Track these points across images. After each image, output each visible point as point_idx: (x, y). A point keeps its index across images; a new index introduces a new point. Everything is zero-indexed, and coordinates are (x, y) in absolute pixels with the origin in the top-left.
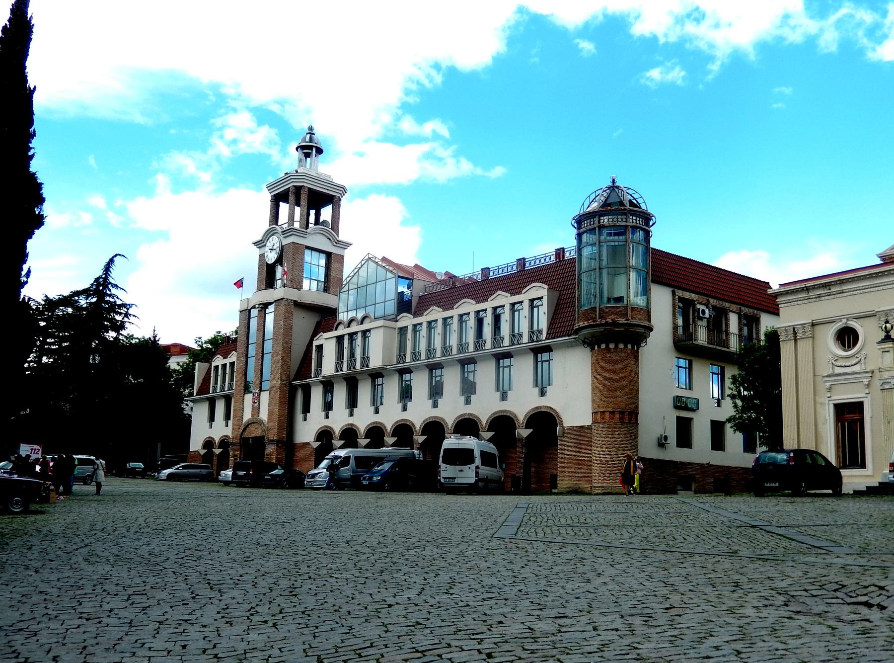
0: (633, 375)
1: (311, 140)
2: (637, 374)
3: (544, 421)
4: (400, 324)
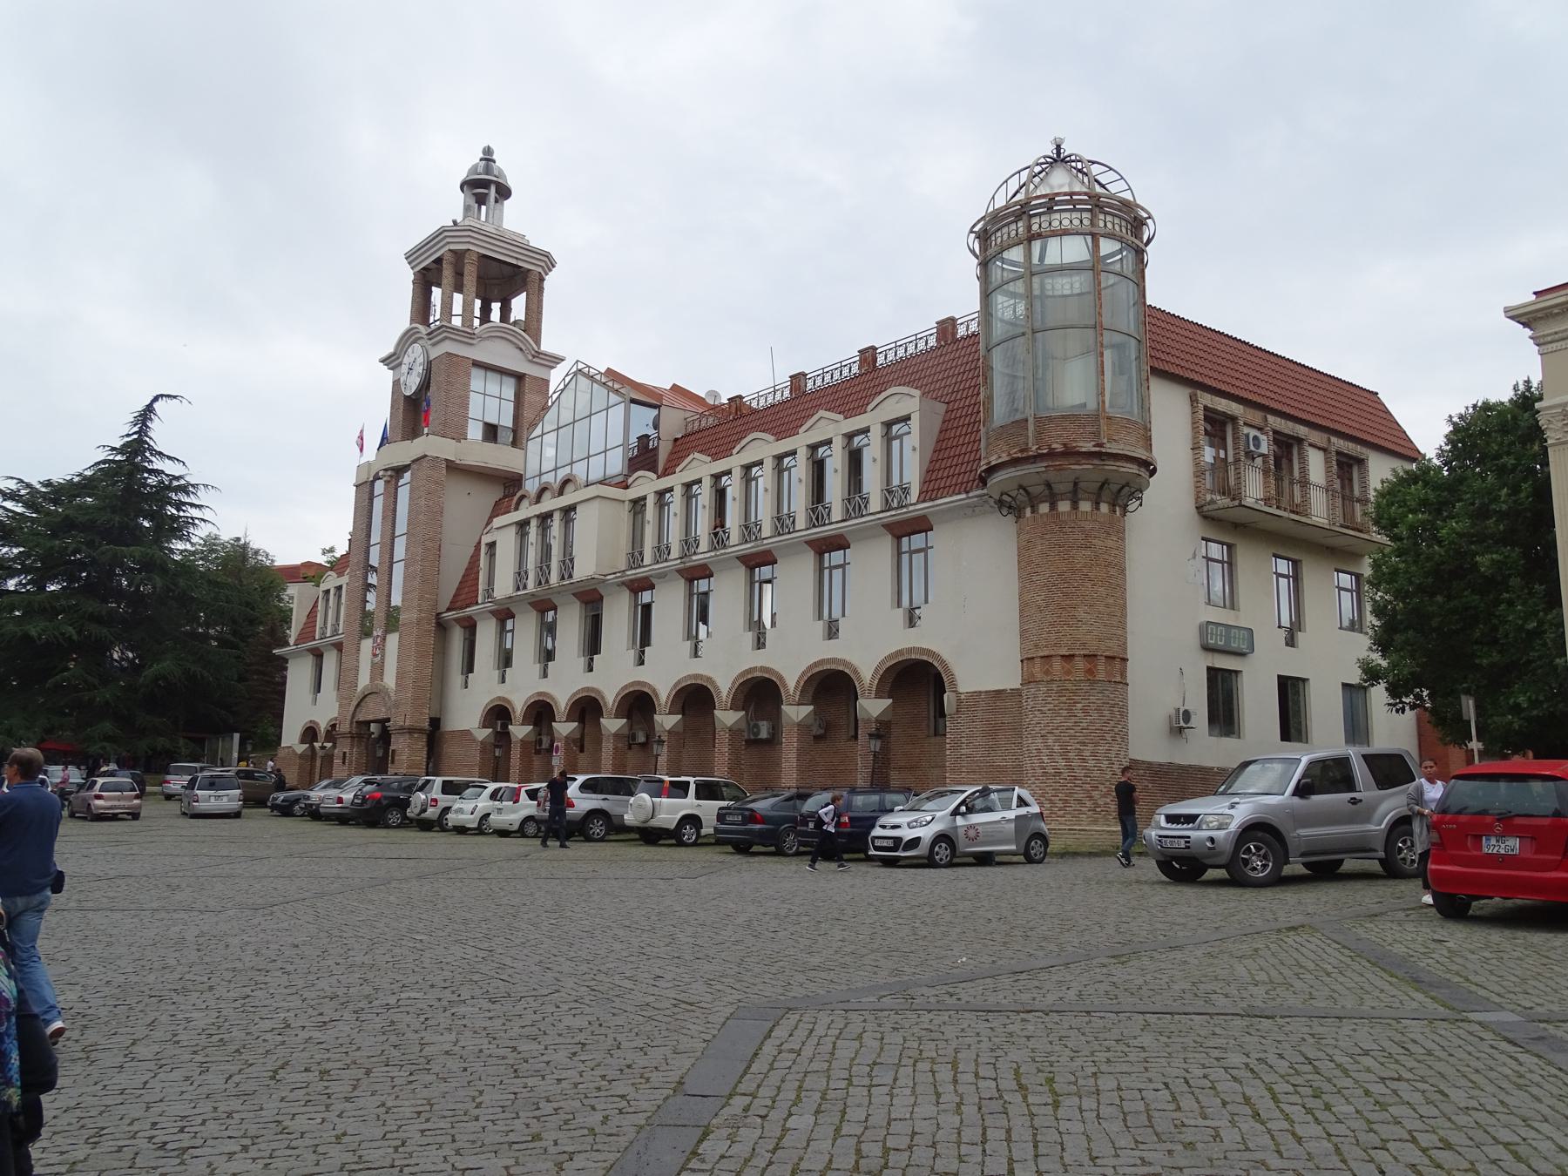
0: (1112, 571)
1: (488, 170)
2: (1122, 571)
3: (916, 679)
4: (633, 493)
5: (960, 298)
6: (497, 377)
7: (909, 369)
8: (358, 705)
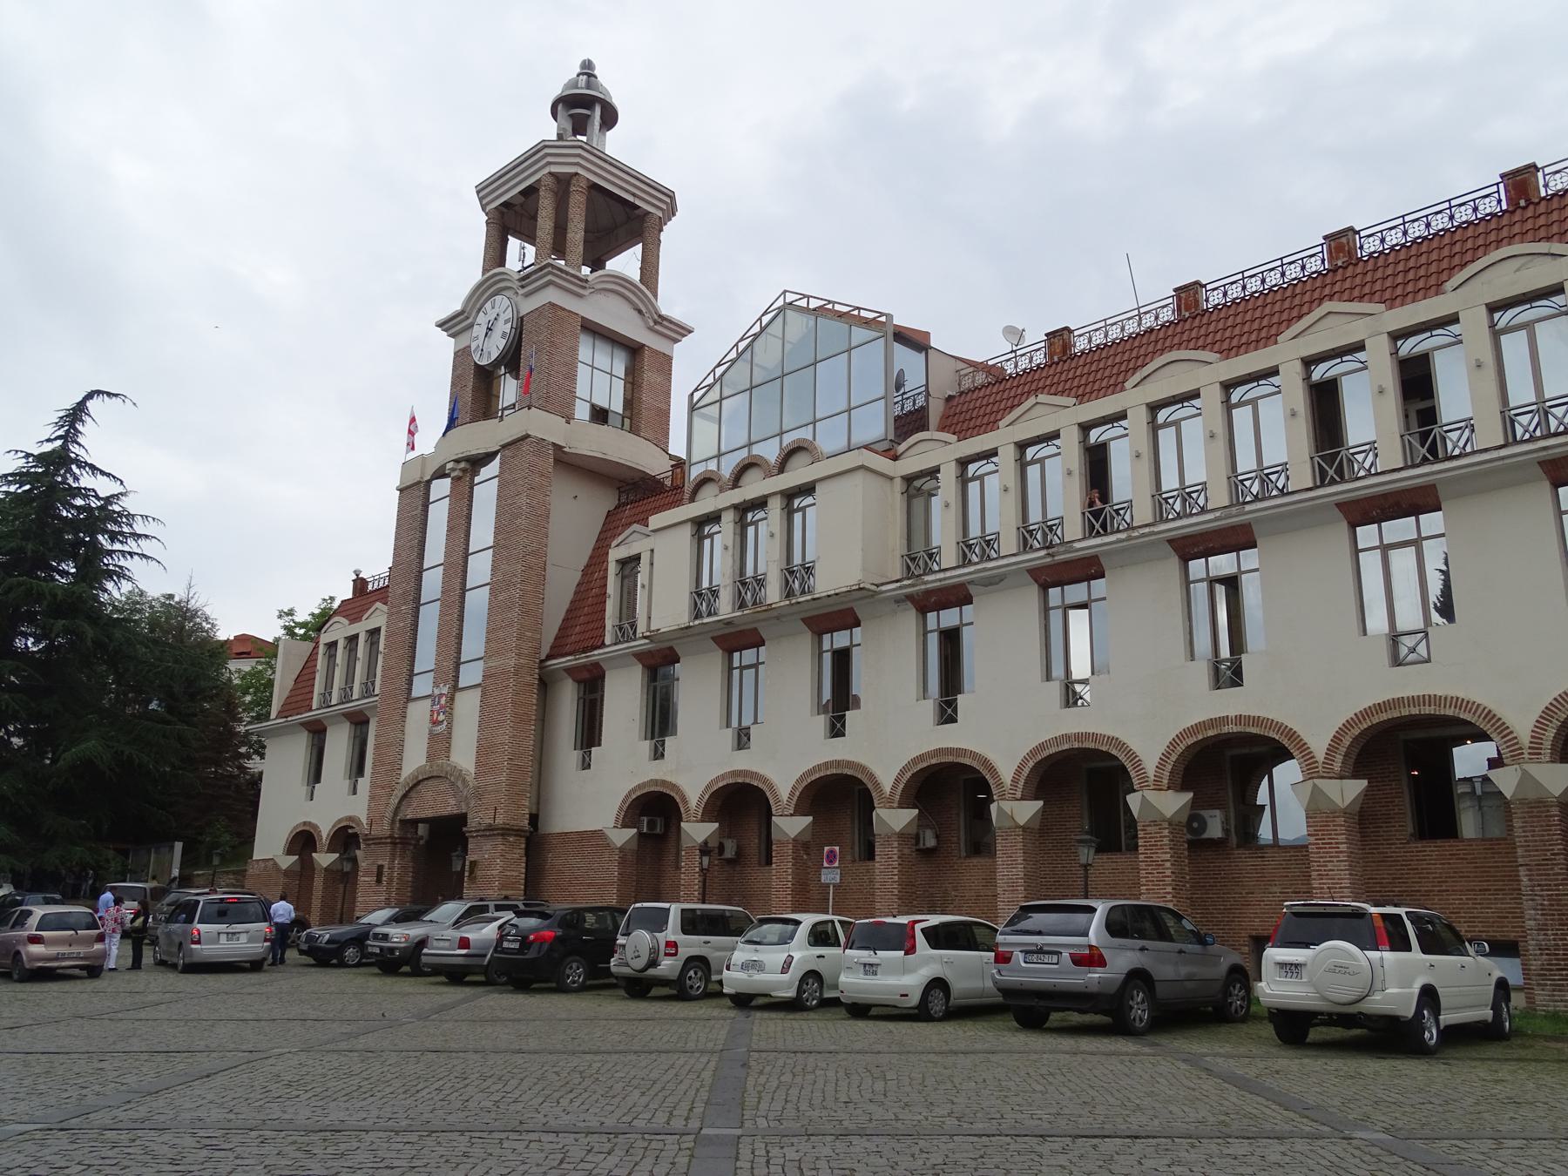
4: (912, 463)
6: (607, 348)
8: (405, 796)
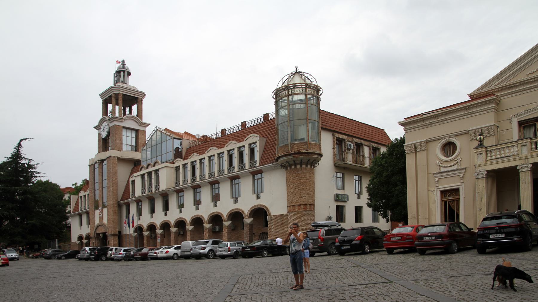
0: (311, 183)
2: (314, 182)
3: (259, 213)
4: (176, 165)
5: (271, 109)
7: (256, 129)
